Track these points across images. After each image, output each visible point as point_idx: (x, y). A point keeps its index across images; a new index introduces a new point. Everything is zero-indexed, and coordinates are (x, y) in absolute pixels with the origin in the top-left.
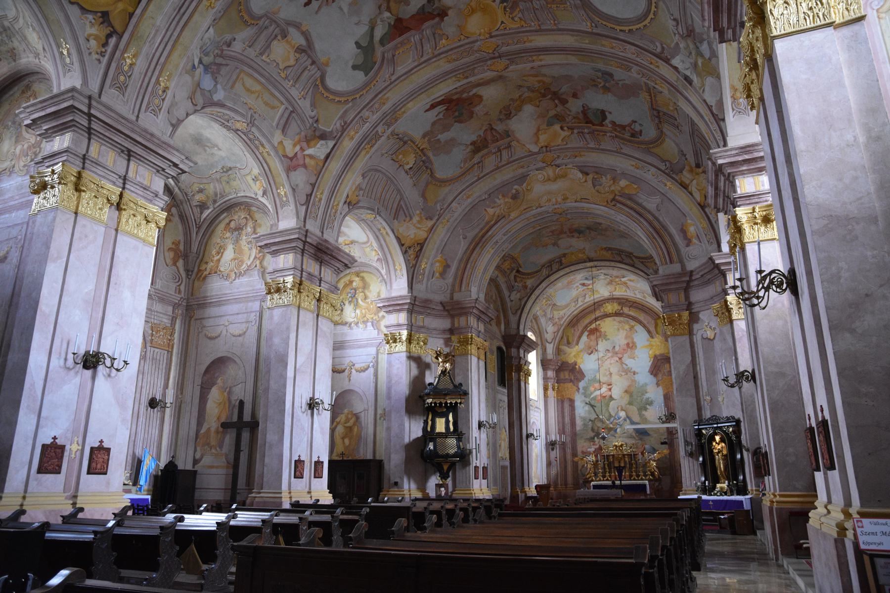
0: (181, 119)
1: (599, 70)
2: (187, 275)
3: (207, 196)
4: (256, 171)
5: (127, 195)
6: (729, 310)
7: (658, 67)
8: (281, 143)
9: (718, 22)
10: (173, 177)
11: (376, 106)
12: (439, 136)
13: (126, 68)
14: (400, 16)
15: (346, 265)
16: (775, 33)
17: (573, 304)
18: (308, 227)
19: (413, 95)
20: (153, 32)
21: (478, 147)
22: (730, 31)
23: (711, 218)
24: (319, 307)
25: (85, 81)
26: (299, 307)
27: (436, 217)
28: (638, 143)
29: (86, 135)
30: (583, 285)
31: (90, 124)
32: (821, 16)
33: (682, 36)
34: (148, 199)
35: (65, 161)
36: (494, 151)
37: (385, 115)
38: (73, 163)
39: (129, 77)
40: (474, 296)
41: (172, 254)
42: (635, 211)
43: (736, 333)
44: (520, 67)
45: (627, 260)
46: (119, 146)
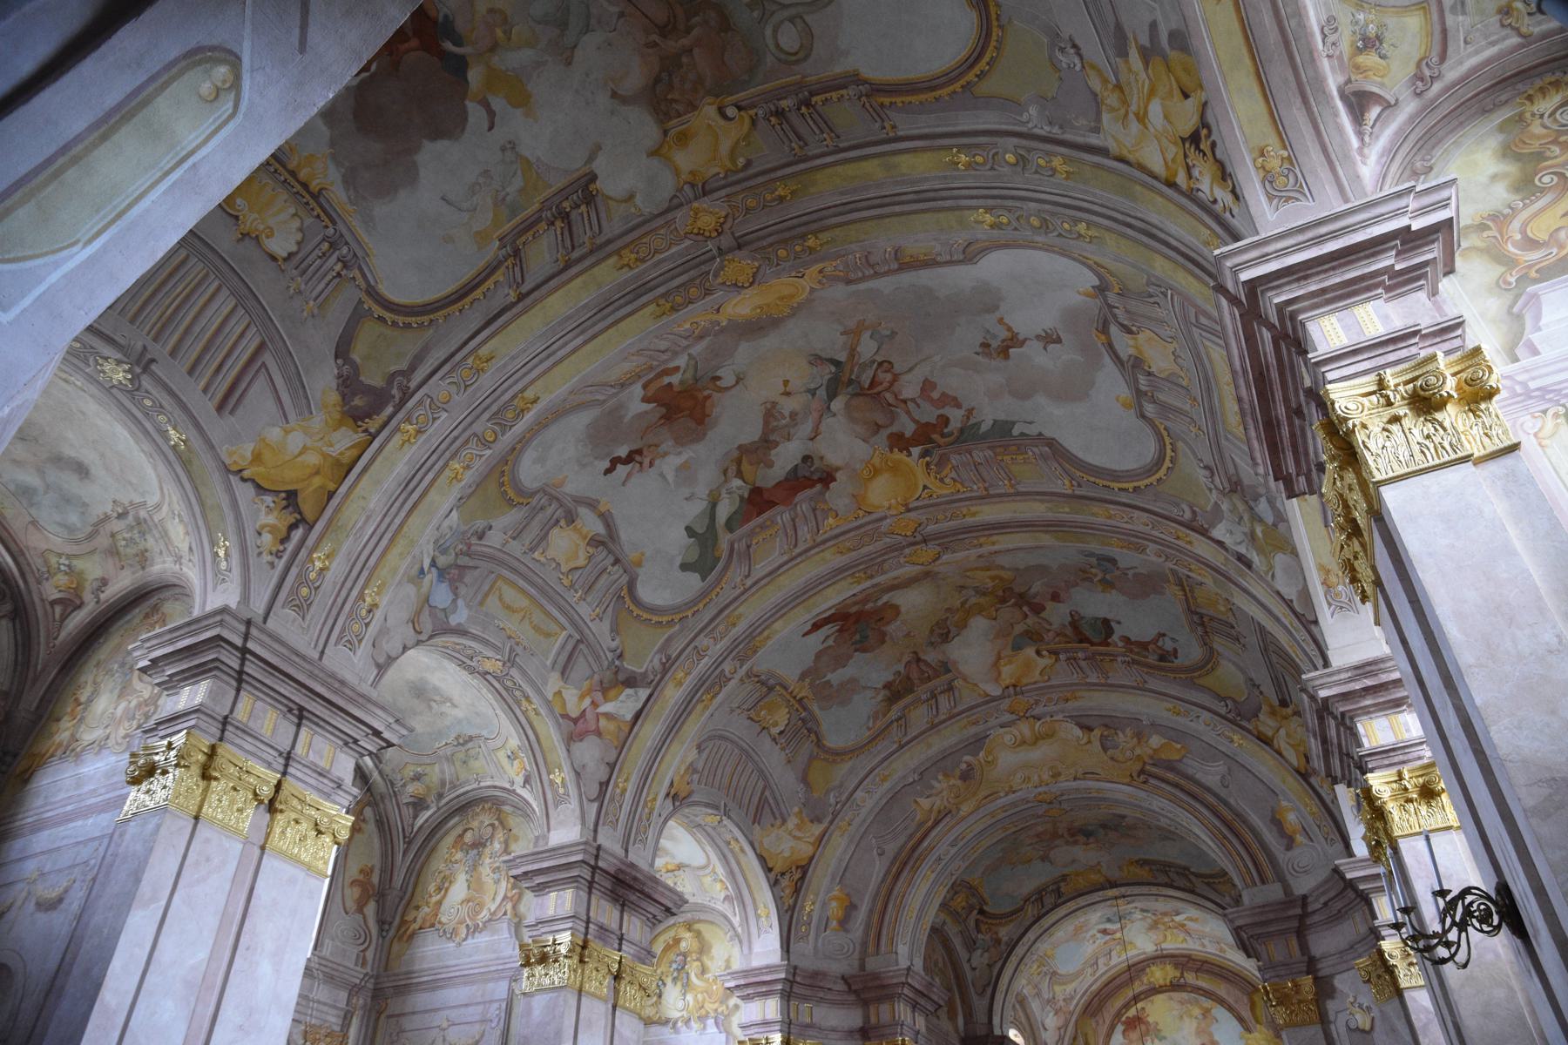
0: (393, 654)
1: (1091, 554)
2: (381, 930)
3: (427, 787)
4: (514, 742)
5: (290, 785)
6: (1390, 970)
7: (1190, 543)
8: (559, 693)
9: (1279, 466)
10: (371, 754)
11: (721, 628)
12: (829, 676)
13: (313, 575)
15: (668, 910)
16: (1378, 477)
17: (1090, 970)
18: (601, 840)
19: (781, 610)
20: (363, 519)
21: (896, 692)
22: (1302, 479)
23: (1324, 795)
24: (616, 991)
25: (245, 597)
26: (580, 991)
27: (830, 818)
28: (1173, 670)
29: (234, 683)
30: (1104, 932)
31: (242, 665)
32: (1448, 448)
33: (1222, 492)
34: (325, 793)
35: (193, 727)
36: (924, 697)
37: (736, 643)
38: (204, 731)
39: (317, 588)
40: (904, 963)
41: (356, 892)
42: (1182, 790)
43: (1413, 1017)
44: (960, 555)
45: (1181, 882)
46: (285, 702)
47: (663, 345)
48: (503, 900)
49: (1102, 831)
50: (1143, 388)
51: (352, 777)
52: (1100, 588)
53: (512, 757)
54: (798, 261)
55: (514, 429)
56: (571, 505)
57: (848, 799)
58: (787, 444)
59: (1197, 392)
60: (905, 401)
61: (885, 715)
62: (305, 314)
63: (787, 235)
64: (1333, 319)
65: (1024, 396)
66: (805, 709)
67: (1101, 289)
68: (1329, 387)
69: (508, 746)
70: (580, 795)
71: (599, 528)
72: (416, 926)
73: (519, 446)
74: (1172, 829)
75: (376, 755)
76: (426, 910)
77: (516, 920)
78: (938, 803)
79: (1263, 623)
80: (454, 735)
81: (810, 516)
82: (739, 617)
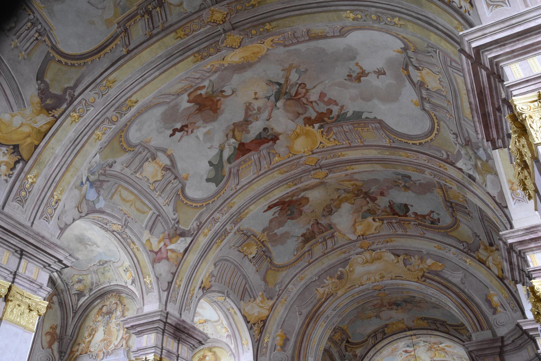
0: (68, 223)
1: (399, 174)
2: (60, 356)
5: (15, 287)
7: (446, 169)
8: (148, 240)
9: (489, 134)
10: (57, 271)
11: (225, 209)
12: (276, 231)
14: (243, 141)
19: (254, 200)
21: (307, 238)
22: (500, 141)
23: (511, 289)
27: (276, 297)
28: (438, 228)
30: (406, 352)
33: (462, 146)
36: (320, 240)
37: (232, 216)
39: (29, 192)
41: (49, 338)
42: (443, 285)
45: (443, 328)
46: (14, 247)
47: (198, 76)
48: (121, 339)
49: (404, 304)
50: (425, 96)
51: (47, 282)
52: (403, 189)
53: (126, 271)
54: (261, 36)
55: (126, 115)
56: (154, 151)
57: (285, 288)
58: (256, 122)
59: (450, 97)
60: (311, 102)
61: (302, 249)
62: (20, 58)
63: (256, 23)
64: (517, 65)
65: (367, 99)
66: (265, 246)
67: (405, 49)
68: (513, 98)
69: (124, 265)
70: (159, 289)
71: (168, 162)
72: (78, 353)
73: (129, 124)
74: (438, 303)
75: (60, 272)
76: (83, 345)
77: (127, 349)
78: (327, 290)
79: (481, 207)
80: (98, 261)
81: (267, 156)
82: (234, 203)
